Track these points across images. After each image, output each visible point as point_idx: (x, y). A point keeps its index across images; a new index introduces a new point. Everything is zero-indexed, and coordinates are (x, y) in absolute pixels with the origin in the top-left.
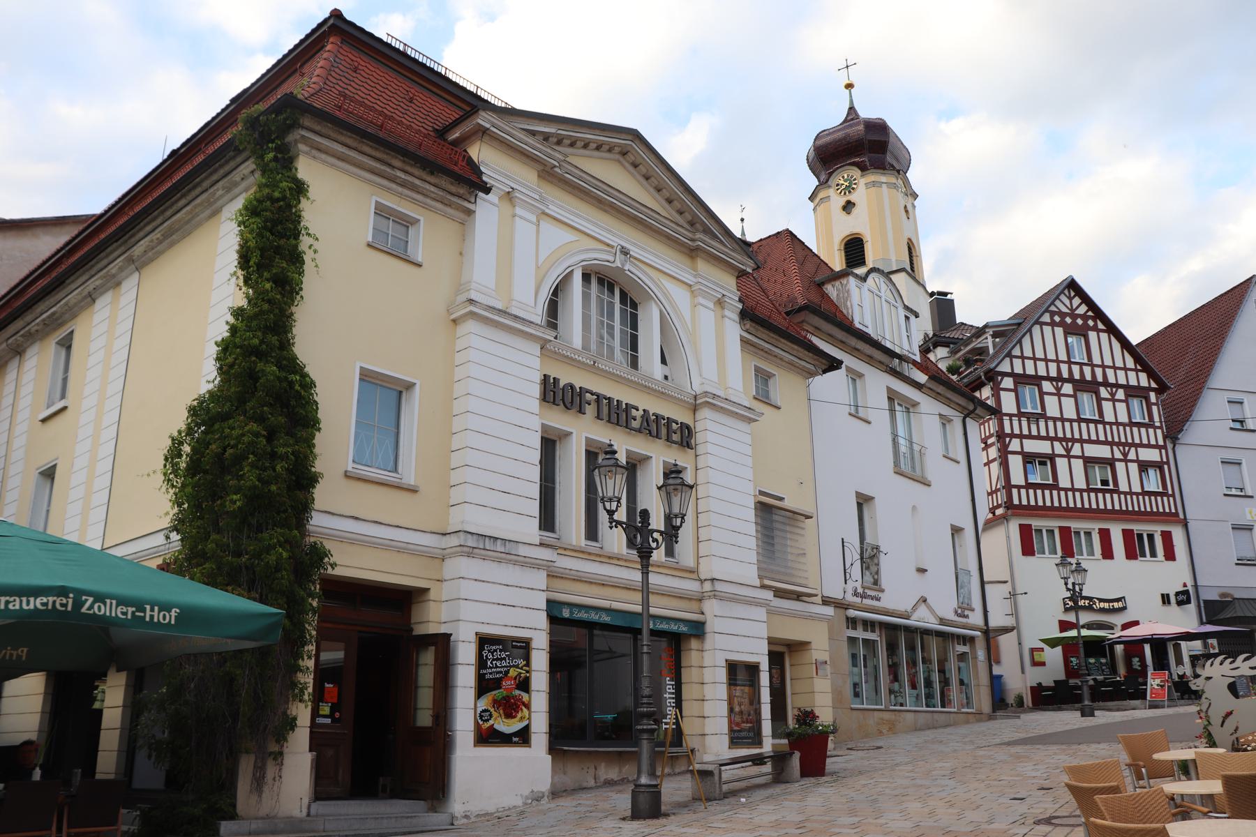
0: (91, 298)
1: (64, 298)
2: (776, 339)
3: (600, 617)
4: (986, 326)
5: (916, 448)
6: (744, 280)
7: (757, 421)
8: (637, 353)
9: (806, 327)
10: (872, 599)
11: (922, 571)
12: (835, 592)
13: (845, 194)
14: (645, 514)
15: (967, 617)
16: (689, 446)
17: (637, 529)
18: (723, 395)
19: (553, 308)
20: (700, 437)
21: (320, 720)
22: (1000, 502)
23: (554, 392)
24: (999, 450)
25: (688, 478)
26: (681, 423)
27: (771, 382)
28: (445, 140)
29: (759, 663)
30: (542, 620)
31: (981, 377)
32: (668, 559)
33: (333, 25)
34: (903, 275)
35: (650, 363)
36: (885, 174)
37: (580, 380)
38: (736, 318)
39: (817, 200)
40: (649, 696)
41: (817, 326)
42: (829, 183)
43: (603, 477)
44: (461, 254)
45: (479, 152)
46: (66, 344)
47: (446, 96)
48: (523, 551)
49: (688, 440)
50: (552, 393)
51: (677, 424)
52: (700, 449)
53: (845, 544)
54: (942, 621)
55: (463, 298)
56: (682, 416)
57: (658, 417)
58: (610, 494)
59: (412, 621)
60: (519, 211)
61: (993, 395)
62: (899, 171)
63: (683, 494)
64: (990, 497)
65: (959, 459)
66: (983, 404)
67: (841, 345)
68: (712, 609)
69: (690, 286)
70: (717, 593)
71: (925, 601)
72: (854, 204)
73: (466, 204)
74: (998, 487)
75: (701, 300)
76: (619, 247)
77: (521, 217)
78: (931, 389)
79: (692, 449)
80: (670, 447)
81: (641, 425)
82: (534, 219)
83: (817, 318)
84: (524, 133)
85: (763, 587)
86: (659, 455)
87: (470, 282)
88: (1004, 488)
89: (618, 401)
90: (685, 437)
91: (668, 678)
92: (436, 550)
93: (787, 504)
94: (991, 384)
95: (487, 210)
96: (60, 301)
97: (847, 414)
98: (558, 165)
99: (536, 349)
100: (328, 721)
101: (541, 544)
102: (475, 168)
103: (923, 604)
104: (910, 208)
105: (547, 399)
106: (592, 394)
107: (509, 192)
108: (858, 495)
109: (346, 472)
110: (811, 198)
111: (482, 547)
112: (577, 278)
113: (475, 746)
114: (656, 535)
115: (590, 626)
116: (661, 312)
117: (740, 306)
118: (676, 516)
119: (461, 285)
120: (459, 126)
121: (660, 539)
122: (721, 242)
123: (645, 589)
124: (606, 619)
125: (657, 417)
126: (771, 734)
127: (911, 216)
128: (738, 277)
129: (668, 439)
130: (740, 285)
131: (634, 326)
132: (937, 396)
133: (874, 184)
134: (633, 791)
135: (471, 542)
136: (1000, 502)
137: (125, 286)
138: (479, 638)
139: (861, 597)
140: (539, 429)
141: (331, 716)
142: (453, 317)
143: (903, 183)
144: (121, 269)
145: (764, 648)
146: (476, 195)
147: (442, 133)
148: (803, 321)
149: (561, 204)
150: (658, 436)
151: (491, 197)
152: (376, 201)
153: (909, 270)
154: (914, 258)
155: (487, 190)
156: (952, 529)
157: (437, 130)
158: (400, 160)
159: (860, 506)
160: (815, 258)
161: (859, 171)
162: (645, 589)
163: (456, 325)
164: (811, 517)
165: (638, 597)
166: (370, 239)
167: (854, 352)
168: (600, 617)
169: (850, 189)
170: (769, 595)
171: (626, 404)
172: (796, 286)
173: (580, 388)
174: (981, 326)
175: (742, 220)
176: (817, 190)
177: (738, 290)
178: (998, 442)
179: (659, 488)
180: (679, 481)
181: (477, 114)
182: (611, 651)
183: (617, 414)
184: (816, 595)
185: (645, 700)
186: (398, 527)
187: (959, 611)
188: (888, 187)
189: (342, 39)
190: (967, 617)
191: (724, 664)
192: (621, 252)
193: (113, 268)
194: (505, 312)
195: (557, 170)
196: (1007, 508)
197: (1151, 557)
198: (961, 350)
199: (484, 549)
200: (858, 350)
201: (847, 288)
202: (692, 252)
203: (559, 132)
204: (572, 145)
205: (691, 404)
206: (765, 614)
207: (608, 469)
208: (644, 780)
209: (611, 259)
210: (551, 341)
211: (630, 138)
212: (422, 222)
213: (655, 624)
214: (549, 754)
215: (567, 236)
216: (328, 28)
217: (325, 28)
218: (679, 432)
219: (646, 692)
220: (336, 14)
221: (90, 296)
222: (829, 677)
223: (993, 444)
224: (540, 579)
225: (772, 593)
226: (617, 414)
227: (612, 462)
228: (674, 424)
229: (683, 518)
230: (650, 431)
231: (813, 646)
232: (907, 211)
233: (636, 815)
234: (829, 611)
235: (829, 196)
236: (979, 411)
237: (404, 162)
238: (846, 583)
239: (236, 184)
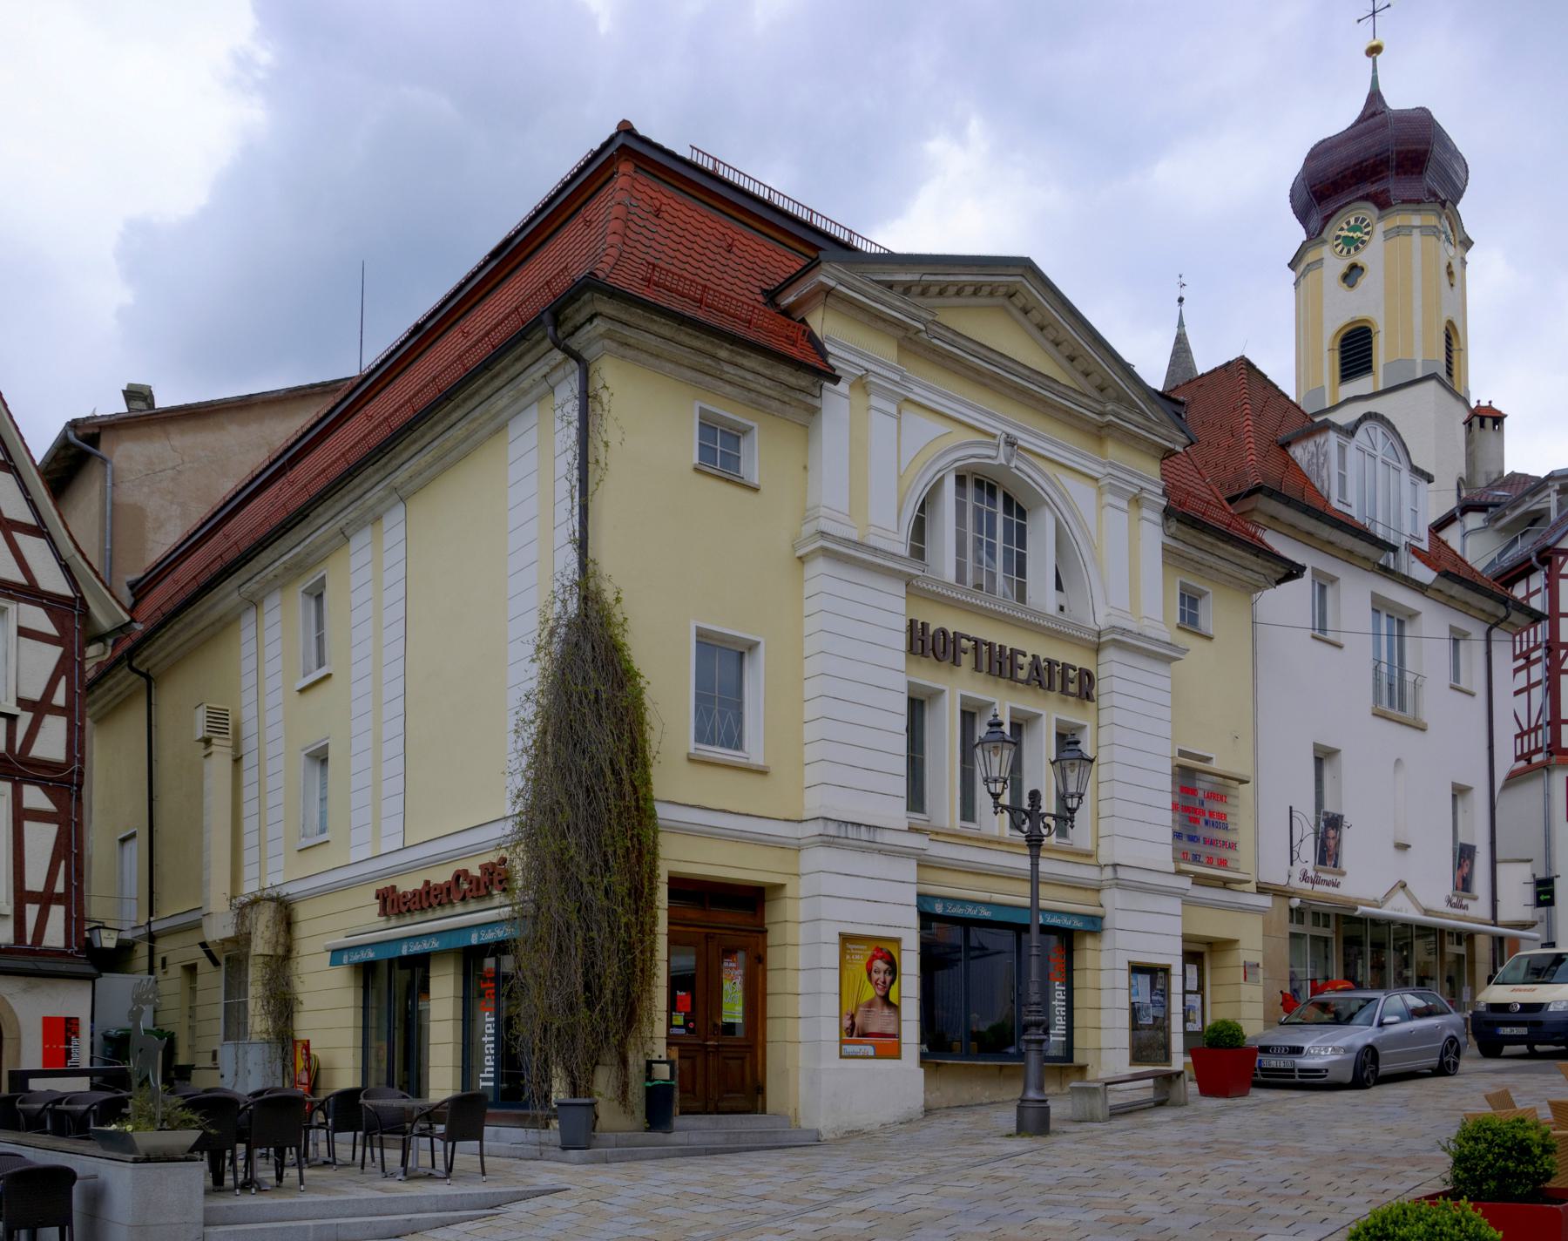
0: (344, 536)
1: (309, 536)
2: (1212, 544)
4: (1550, 477)
5: (1409, 677)
6: (1178, 461)
8: (1025, 578)
9: (1256, 517)
10: (1328, 884)
11: (1403, 847)
12: (1276, 874)
13: (1349, 252)
14: (1035, 796)
15: (1466, 907)
16: (1089, 697)
17: (1025, 814)
18: (1135, 630)
19: (919, 529)
20: (1102, 687)
21: (675, 1031)
22: (1540, 745)
23: (923, 641)
24: (1548, 668)
25: (1087, 748)
26: (1080, 669)
27: (1202, 604)
28: (777, 305)
29: (1170, 966)
30: (913, 919)
31: (1530, 559)
32: (1059, 840)
33: (623, 146)
34: (1433, 384)
35: (1042, 594)
36: (1419, 210)
37: (954, 623)
38: (1157, 518)
39: (1302, 267)
40: (1038, 1004)
41: (1274, 514)
42: (1324, 235)
43: (986, 754)
44: (805, 468)
45: (823, 323)
46: (317, 595)
47: (775, 235)
48: (882, 837)
50: (920, 642)
51: (1075, 670)
52: (1104, 701)
53: (1294, 814)
54: (1427, 912)
55: (809, 529)
56: (1078, 659)
58: (995, 774)
59: (766, 921)
61: (1547, 586)
62: (1445, 201)
63: (1082, 769)
64: (1519, 741)
65: (1474, 690)
66: (1522, 607)
67: (1308, 539)
68: (1113, 904)
69: (1096, 480)
70: (1119, 882)
71: (1404, 886)
72: (1362, 269)
73: (809, 400)
74: (1540, 722)
75: (1109, 499)
76: (1004, 436)
77: (877, 409)
78: (1440, 591)
79: (1093, 701)
80: (1065, 701)
81: (1029, 676)
82: (893, 409)
83: (1273, 503)
84: (879, 287)
85: (1179, 873)
86: (1050, 713)
87: (818, 506)
88: (1548, 724)
89: (1000, 646)
90: (1084, 687)
91: (1057, 983)
92: (791, 841)
93: (1215, 766)
94: (1547, 568)
95: (836, 402)
96: (304, 540)
97: (1310, 638)
98: (923, 328)
99: (901, 589)
100: (683, 1031)
102: (817, 346)
103: (1401, 891)
104: (1456, 268)
105: (914, 651)
106: (969, 639)
107: (861, 377)
108: (1317, 747)
109: (688, 754)
110: (1293, 265)
111: (843, 835)
112: (950, 484)
114: (1048, 820)
115: (967, 923)
118: (1072, 796)
119: (808, 510)
120: (794, 286)
121: (1053, 824)
122: (1142, 413)
123: (1035, 879)
124: (985, 914)
125: (1049, 663)
126: (1182, 1050)
127: (1457, 282)
129: (1064, 691)
130: (1166, 472)
131: (1022, 543)
132: (1449, 601)
133: (1399, 231)
134: (1018, 1106)
135: (832, 830)
136: (1540, 745)
137: (388, 521)
139: (1313, 882)
140: (904, 689)
141: (685, 1026)
142: (799, 554)
143: (1450, 224)
144: (381, 500)
145: (1178, 948)
146: (821, 386)
147: (772, 296)
148: (1253, 510)
149: (930, 385)
150: (1050, 688)
151: (842, 387)
152: (700, 408)
153: (1444, 375)
154: (1455, 354)
155: (836, 380)
156: (1453, 789)
157: (765, 290)
158: (727, 349)
159: (1319, 762)
160: (1282, 399)
161: (1376, 210)
162: (1035, 879)
163: (803, 562)
164: (1247, 782)
166: (696, 460)
167: (1326, 547)
169: (1353, 244)
170: (1185, 883)
171: (1011, 649)
172: (1248, 453)
173: (954, 633)
174: (1543, 475)
175: (1181, 300)
176: (1303, 249)
177: (1163, 480)
178: (1547, 655)
179: (1053, 763)
180: (1077, 754)
181: (818, 268)
182: (982, 948)
183: (999, 664)
184: (1249, 882)
185: (1034, 1008)
186: (747, 815)
187: (1455, 900)
188: (1422, 234)
189: (636, 166)
190: (1466, 907)
191: (836, 939)
192: (1006, 442)
193: (371, 499)
194: (862, 545)
195: (924, 335)
196: (1551, 753)
198: (1504, 516)
199: (847, 838)
200: (1331, 543)
201: (1324, 450)
202: (1100, 433)
203: (925, 278)
204: (941, 293)
205: (1093, 643)
207: (992, 745)
208: (1032, 1094)
209: (992, 453)
210: (918, 576)
211: (1019, 271)
212: (756, 429)
213: (1045, 919)
214: (921, 1067)
215: (937, 427)
216: (617, 150)
217: (611, 150)
218: (1077, 681)
219: (1035, 998)
220: (626, 129)
221: (343, 533)
222: (1261, 983)
223: (1538, 660)
224: (909, 870)
225: (1189, 881)
226: (999, 664)
227: (998, 736)
228: (1071, 671)
229: (1080, 798)
230: (1040, 682)
231: (1242, 944)
232: (1450, 274)
233: (1022, 1130)
234: (1265, 901)
235: (1322, 259)
236: (1515, 617)
237: (732, 351)
238: (1292, 864)
239: (525, 393)
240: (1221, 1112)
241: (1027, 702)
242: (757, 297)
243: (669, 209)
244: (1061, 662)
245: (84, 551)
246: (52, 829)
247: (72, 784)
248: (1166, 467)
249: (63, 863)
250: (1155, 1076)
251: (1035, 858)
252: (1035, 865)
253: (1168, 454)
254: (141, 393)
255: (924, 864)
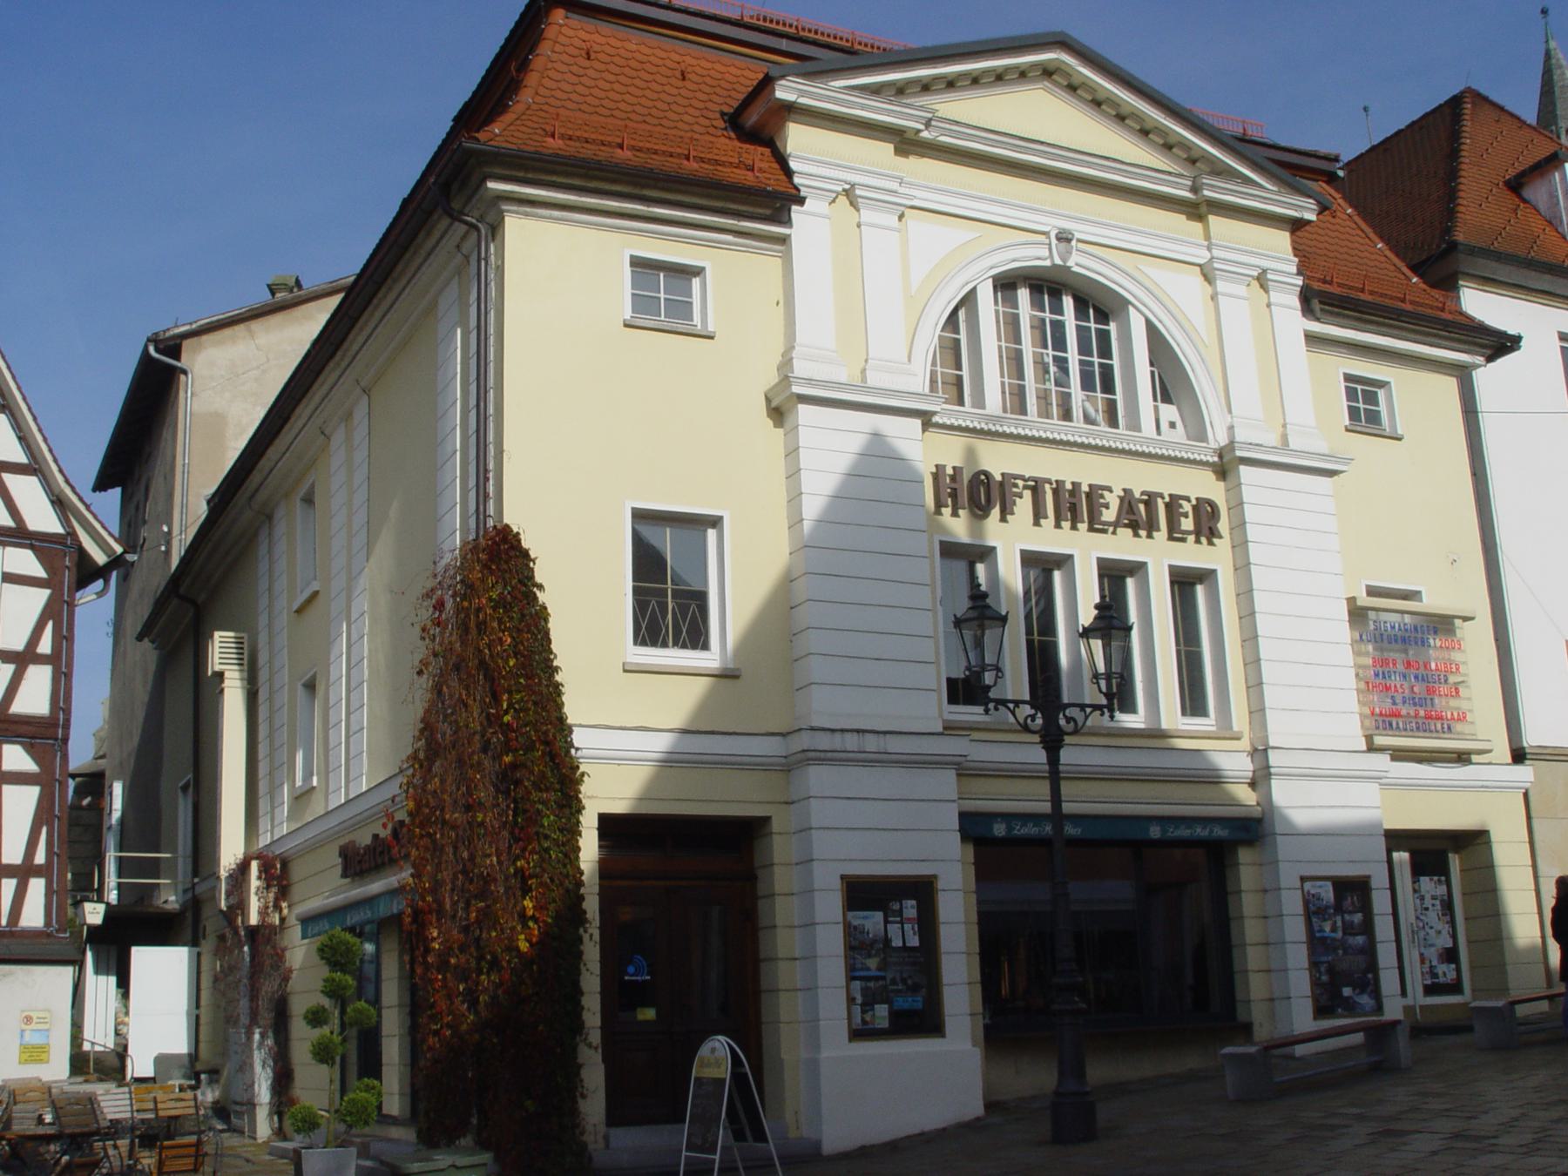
3: (1211, 831)
7: (1342, 472)
19: (951, 351)
29: (1369, 877)
38: (1296, 302)
51: (1051, 484)
57: (1150, 499)
60: (866, 215)
85: (1372, 748)
101: (945, 728)
112: (986, 295)
116: (1149, 323)
117: (1299, 281)
128: (1293, 232)
162: (1055, 774)
165: (1044, 788)
168: (1211, 831)
170: (1382, 761)
191: (837, 884)
197: (973, 406)
240: (230, 1137)
242: (714, 123)
245: (74, 484)
246: (33, 792)
247: (56, 739)
248: (1298, 240)
249: (44, 830)
250: (1367, 1029)
252: (1053, 760)
254: (286, 285)
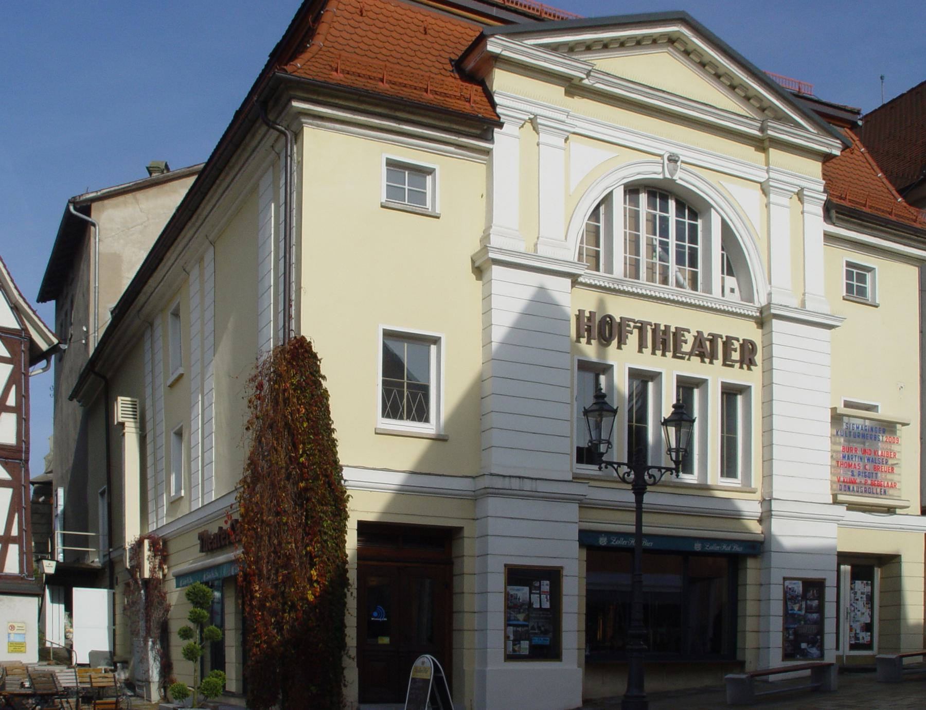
19: (593, 234)
29: (562, 567)
49: (751, 357)
51: (651, 326)
56: (748, 331)
60: (544, 137)
113: (505, 661)
128: (824, 163)
138: (508, 569)
162: (639, 509)
165: (632, 517)
168: (732, 548)
170: (841, 510)
177: (824, 179)
191: (502, 569)
195: (586, 82)
197: (704, 291)
206: (578, 508)
224: (572, 511)
241: (693, 368)
242: (445, 67)
243: (435, 27)
244: (653, 323)
251: (639, 489)
252: (639, 500)
253: (826, 158)
255: (585, 505)
